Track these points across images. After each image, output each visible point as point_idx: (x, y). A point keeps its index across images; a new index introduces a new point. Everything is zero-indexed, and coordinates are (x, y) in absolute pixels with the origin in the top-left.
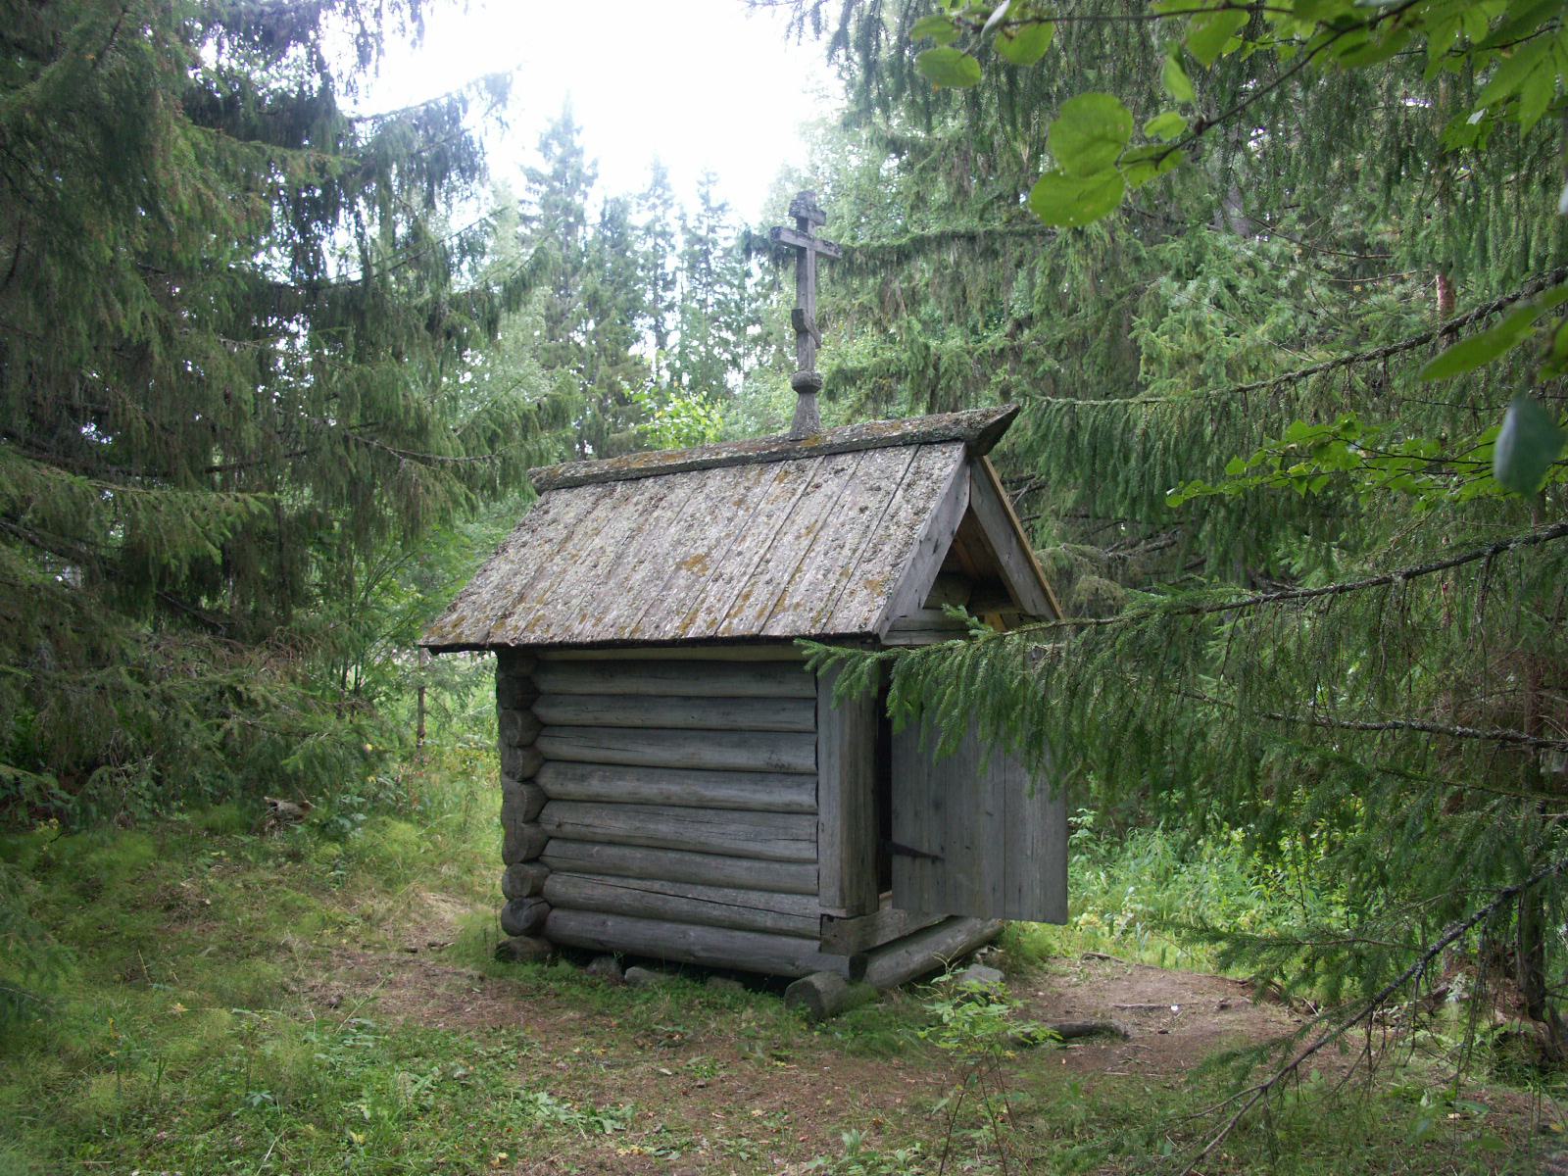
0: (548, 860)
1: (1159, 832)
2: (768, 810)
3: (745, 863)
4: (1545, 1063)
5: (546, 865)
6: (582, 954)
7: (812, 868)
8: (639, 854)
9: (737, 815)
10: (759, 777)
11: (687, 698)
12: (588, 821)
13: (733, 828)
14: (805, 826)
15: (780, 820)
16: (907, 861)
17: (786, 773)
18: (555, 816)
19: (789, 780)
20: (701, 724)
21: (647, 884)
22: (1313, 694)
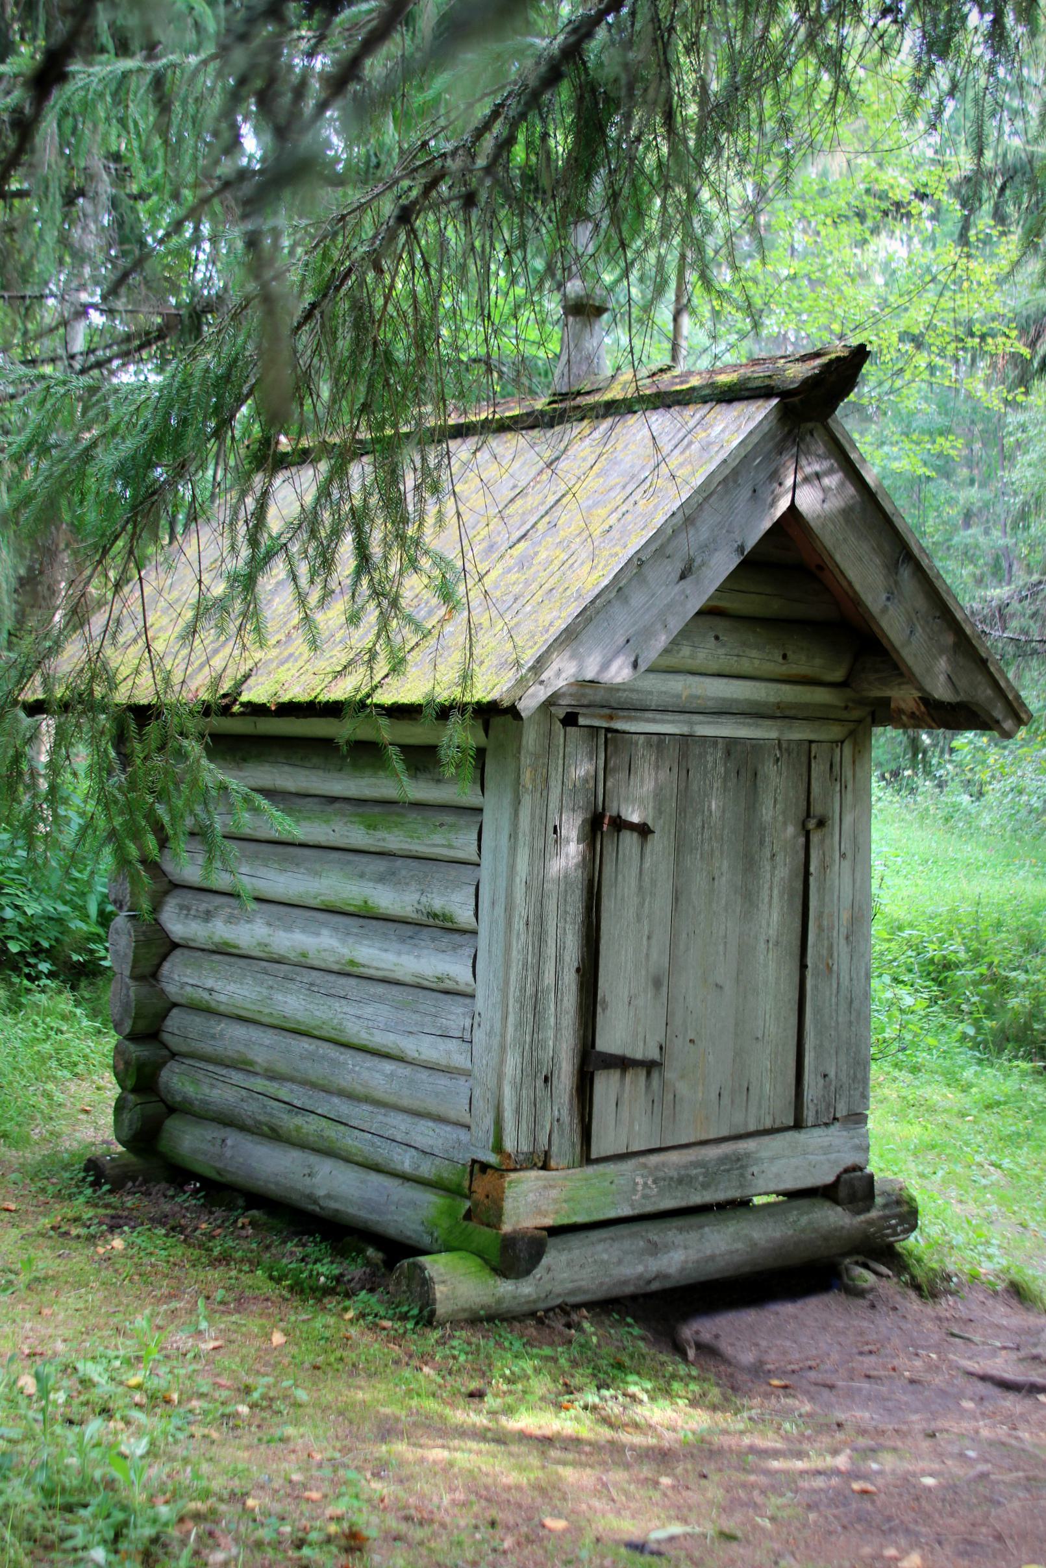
0: (166, 1037)
1: (15, 1233)
2: (507, 982)
3: (388, 1066)
4: (858, 7)
5: (166, 1046)
6: (224, 1194)
7: (462, 1084)
8: (268, 1038)
9: (380, 989)
10: (408, 930)
11: (333, 800)
12: (210, 983)
13: (368, 1011)
14: (455, 1016)
15: (428, 1002)
16: (615, 1075)
17: (440, 926)
18: (180, 978)
19: (447, 938)
20: (341, 843)
21: (272, 1088)
22: (311, 55)
